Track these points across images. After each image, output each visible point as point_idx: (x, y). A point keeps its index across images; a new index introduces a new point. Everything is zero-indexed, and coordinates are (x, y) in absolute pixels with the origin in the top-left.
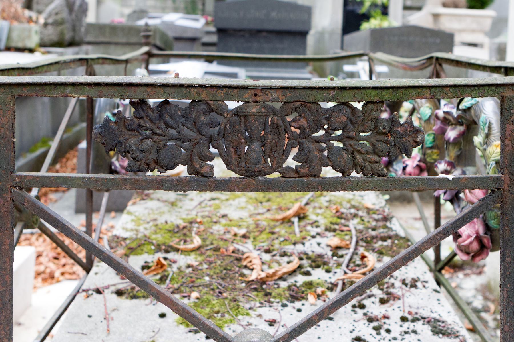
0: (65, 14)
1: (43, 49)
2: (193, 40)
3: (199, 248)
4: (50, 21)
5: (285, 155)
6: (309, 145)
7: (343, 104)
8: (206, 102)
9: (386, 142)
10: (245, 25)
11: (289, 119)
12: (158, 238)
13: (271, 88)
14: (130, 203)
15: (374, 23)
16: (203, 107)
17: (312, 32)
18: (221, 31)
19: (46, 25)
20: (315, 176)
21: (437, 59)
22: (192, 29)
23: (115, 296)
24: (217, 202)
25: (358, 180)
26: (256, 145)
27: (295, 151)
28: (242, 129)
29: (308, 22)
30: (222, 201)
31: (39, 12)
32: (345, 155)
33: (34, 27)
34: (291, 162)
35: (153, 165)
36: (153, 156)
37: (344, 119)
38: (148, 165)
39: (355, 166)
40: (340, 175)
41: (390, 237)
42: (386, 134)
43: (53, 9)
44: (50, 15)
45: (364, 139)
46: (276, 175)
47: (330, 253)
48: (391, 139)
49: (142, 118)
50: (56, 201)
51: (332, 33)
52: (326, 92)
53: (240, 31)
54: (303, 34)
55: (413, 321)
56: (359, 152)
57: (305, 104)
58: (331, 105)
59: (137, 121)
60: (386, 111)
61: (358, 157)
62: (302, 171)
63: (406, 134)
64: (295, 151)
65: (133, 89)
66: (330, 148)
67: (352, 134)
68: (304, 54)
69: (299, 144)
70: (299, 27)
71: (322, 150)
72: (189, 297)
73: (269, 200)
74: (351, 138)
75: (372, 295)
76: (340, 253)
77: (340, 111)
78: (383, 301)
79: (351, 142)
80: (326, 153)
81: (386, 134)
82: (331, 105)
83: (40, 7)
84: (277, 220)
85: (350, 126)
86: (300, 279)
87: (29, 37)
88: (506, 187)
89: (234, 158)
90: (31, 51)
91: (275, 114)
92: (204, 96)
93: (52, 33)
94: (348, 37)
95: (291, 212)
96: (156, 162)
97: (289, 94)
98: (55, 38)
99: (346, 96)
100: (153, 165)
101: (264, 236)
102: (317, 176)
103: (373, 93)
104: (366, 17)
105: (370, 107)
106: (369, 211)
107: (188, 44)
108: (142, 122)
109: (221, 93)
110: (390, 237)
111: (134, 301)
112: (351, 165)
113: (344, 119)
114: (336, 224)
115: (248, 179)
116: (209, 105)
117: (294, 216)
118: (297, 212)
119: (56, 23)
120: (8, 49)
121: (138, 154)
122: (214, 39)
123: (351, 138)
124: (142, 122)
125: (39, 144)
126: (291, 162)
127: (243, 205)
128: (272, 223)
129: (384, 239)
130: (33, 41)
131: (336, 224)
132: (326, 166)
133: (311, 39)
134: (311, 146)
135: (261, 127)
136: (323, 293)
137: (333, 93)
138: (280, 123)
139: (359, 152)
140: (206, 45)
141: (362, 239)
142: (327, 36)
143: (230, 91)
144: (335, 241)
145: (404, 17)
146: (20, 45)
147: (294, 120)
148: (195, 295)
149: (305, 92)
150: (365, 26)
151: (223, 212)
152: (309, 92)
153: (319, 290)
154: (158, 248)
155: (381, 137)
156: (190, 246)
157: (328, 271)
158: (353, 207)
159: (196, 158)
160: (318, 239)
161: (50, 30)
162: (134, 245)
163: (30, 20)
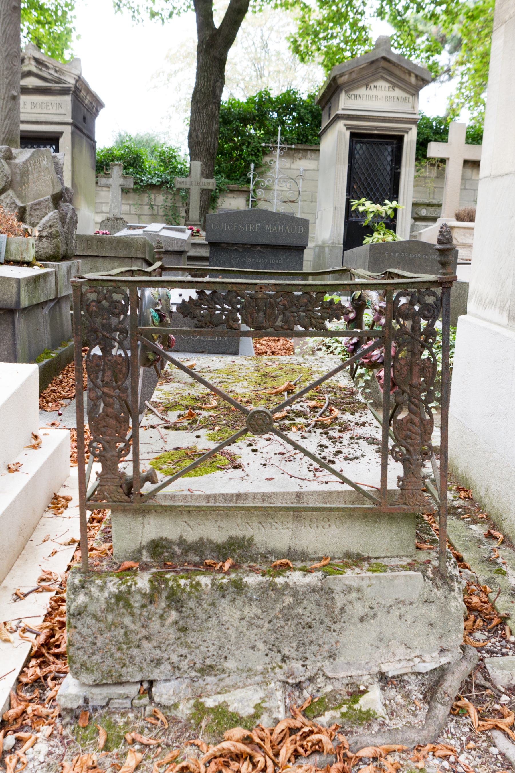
0: (58, 227)
1: (39, 263)
2: (180, 253)
3: (216, 407)
4: (45, 234)
5: (276, 318)
6: (287, 314)
7: (305, 293)
8: (236, 291)
9: (327, 313)
10: (238, 239)
11: (279, 300)
12: (184, 403)
13: (269, 285)
14: (158, 384)
15: (377, 237)
16: (234, 294)
17: (311, 245)
18: (213, 245)
19: (41, 237)
20: (291, 330)
21: (390, 273)
22: (178, 240)
23: (164, 430)
24: (225, 384)
25: (312, 332)
26: (261, 314)
27: (280, 317)
28: (254, 305)
29: (305, 237)
30: (229, 383)
31: (33, 225)
32: (306, 319)
33: (32, 240)
34: (279, 323)
35: (208, 324)
36: (208, 319)
37: (306, 301)
38: (206, 324)
39: (312, 325)
40: (304, 329)
41: (353, 403)
42: (327, 309)
43: (48, 222)
44: (44, 229)
45: (318, 311)
46: (271, 330)
47: (309, 410)
48: (329, 311)
49: (202, 300)
50: (66, 406)
51: (333, 247)
52: (296, 287)
53: (234, 244)
54: (300, 249)
55: (357, 439)
56: (313, 318)
57: (287, 293)
58: (300, 293)
59: (199, 301)
60: (353, 312)
61: (313, 320)
62: (285, 327)
63: (338, 309)
64: (280, 317)
65: (199, 284)
66: (298, 316)
67: (310, 308)
68: (301, 270)
69: (283, 313)
70: (295, 242)
71: (294, 317)
72: (213, 429)
73: (265, 383)
74: (310, 311)
75: (334, 429)
76: (316, 410)
77: (304, 297)
78: (340, 431)
79: (310, 313)
80: (297, 318)
81: (327, 309)
82: (300, 293)
83: (33, 220)
84: (272, 394)
85: (309, 304)
86: (287, 422)
87: (27, 250)
88: (386, 335)
89: (250, 320)
90: (29, 264)
91: (271, 298)
92: (235, 288)
93: (47, 246)
94: (348, 252)
95: (282, 387)
96: (210, 322)
97: (278, 287)
98: (50, 251)
99: (308, 289)
100: (208, 324)
101: (262, 402)
102: (292, 330)
103: (321, 287)
104: (370, 230)
105: (319, 294)
106: (341, 389)
107: (174, 257)
108: (202, 302)
109: (244, 287)
110: (353, 403)
111: (177, 431)
112: (309, 324)
113: (306, 301)
114: (315, 396)
115: (258, 331)
116: (237, 293)
117: (284, 391)
118: (286, 387)
119: (50, 236)
120: (7, 262)
121: (201, 318)
122: (205, 252)
123: (310, 311)
124: (202, 302)
125: (43, 355)
126: (279, 323)
127: (246, 386)
128: (268, 395)
129: (348, 404)
130: (30, 256)
131: (315, 396)
132: (297, 325)
133: (308, 255)
134: (289, 315)
135: (264, 305)
136: (302, 427)
137: (300, 287)
138: (274, 302)
139: (313, 318)
140: (191, 258)
141: (333, 404)
142: (327, 250)
143: (248, 286)
144: (313, 403)
145: (413, 228)
146: (18, 258)
147: (281, 301)
148: (217, 428)
149: (286, 287)
150: (368, 240)
151: (231, 389)
152: (288, 287)
153: (299, 426)
154: (186, 407)
155: (325, 310)
156: (209, 406)
157: (306, 419)
158: (330, 387)
159: (231, 320)
160: (301, 404)
161: (45, 242)
162: (169, 406)
163: (26, 233)
